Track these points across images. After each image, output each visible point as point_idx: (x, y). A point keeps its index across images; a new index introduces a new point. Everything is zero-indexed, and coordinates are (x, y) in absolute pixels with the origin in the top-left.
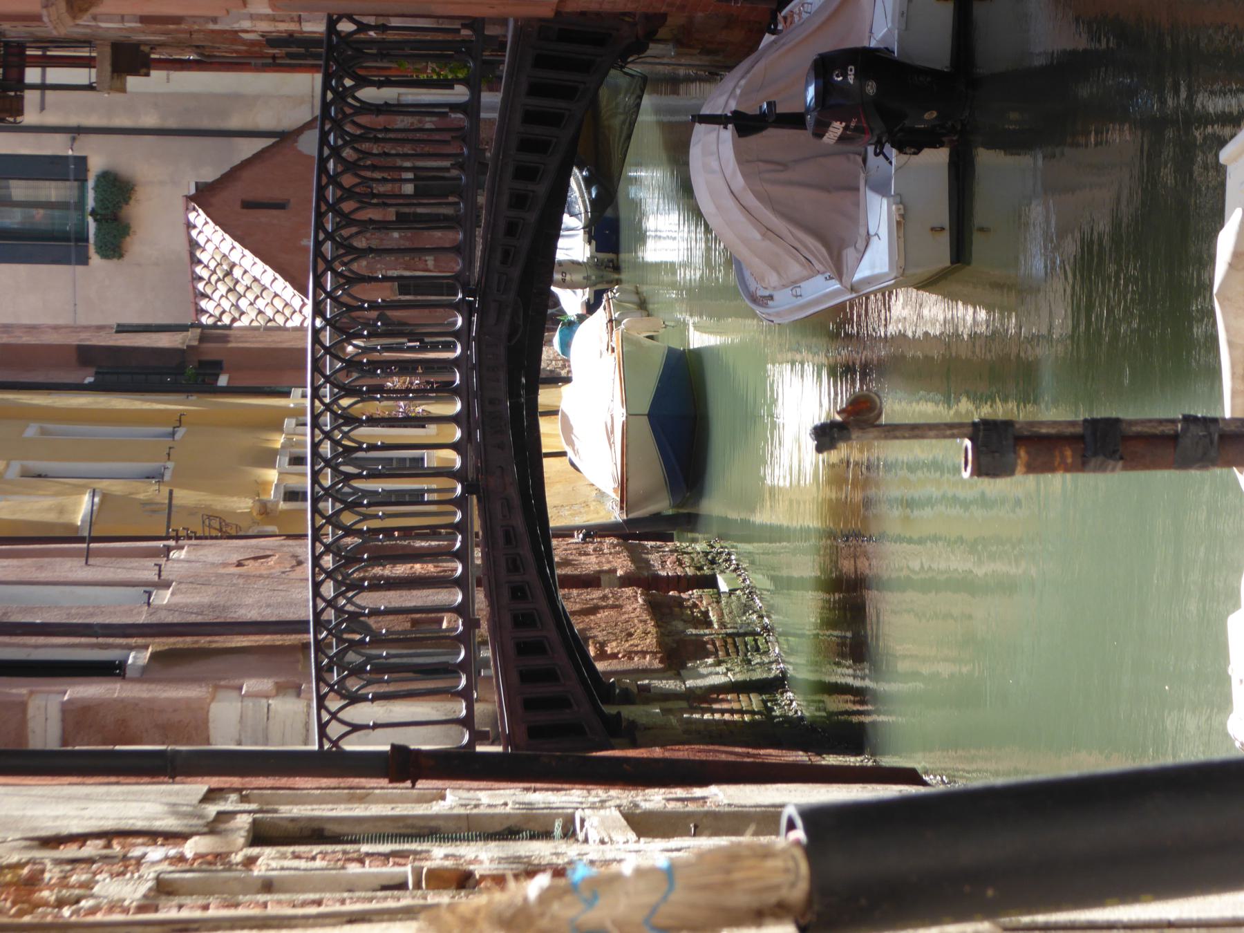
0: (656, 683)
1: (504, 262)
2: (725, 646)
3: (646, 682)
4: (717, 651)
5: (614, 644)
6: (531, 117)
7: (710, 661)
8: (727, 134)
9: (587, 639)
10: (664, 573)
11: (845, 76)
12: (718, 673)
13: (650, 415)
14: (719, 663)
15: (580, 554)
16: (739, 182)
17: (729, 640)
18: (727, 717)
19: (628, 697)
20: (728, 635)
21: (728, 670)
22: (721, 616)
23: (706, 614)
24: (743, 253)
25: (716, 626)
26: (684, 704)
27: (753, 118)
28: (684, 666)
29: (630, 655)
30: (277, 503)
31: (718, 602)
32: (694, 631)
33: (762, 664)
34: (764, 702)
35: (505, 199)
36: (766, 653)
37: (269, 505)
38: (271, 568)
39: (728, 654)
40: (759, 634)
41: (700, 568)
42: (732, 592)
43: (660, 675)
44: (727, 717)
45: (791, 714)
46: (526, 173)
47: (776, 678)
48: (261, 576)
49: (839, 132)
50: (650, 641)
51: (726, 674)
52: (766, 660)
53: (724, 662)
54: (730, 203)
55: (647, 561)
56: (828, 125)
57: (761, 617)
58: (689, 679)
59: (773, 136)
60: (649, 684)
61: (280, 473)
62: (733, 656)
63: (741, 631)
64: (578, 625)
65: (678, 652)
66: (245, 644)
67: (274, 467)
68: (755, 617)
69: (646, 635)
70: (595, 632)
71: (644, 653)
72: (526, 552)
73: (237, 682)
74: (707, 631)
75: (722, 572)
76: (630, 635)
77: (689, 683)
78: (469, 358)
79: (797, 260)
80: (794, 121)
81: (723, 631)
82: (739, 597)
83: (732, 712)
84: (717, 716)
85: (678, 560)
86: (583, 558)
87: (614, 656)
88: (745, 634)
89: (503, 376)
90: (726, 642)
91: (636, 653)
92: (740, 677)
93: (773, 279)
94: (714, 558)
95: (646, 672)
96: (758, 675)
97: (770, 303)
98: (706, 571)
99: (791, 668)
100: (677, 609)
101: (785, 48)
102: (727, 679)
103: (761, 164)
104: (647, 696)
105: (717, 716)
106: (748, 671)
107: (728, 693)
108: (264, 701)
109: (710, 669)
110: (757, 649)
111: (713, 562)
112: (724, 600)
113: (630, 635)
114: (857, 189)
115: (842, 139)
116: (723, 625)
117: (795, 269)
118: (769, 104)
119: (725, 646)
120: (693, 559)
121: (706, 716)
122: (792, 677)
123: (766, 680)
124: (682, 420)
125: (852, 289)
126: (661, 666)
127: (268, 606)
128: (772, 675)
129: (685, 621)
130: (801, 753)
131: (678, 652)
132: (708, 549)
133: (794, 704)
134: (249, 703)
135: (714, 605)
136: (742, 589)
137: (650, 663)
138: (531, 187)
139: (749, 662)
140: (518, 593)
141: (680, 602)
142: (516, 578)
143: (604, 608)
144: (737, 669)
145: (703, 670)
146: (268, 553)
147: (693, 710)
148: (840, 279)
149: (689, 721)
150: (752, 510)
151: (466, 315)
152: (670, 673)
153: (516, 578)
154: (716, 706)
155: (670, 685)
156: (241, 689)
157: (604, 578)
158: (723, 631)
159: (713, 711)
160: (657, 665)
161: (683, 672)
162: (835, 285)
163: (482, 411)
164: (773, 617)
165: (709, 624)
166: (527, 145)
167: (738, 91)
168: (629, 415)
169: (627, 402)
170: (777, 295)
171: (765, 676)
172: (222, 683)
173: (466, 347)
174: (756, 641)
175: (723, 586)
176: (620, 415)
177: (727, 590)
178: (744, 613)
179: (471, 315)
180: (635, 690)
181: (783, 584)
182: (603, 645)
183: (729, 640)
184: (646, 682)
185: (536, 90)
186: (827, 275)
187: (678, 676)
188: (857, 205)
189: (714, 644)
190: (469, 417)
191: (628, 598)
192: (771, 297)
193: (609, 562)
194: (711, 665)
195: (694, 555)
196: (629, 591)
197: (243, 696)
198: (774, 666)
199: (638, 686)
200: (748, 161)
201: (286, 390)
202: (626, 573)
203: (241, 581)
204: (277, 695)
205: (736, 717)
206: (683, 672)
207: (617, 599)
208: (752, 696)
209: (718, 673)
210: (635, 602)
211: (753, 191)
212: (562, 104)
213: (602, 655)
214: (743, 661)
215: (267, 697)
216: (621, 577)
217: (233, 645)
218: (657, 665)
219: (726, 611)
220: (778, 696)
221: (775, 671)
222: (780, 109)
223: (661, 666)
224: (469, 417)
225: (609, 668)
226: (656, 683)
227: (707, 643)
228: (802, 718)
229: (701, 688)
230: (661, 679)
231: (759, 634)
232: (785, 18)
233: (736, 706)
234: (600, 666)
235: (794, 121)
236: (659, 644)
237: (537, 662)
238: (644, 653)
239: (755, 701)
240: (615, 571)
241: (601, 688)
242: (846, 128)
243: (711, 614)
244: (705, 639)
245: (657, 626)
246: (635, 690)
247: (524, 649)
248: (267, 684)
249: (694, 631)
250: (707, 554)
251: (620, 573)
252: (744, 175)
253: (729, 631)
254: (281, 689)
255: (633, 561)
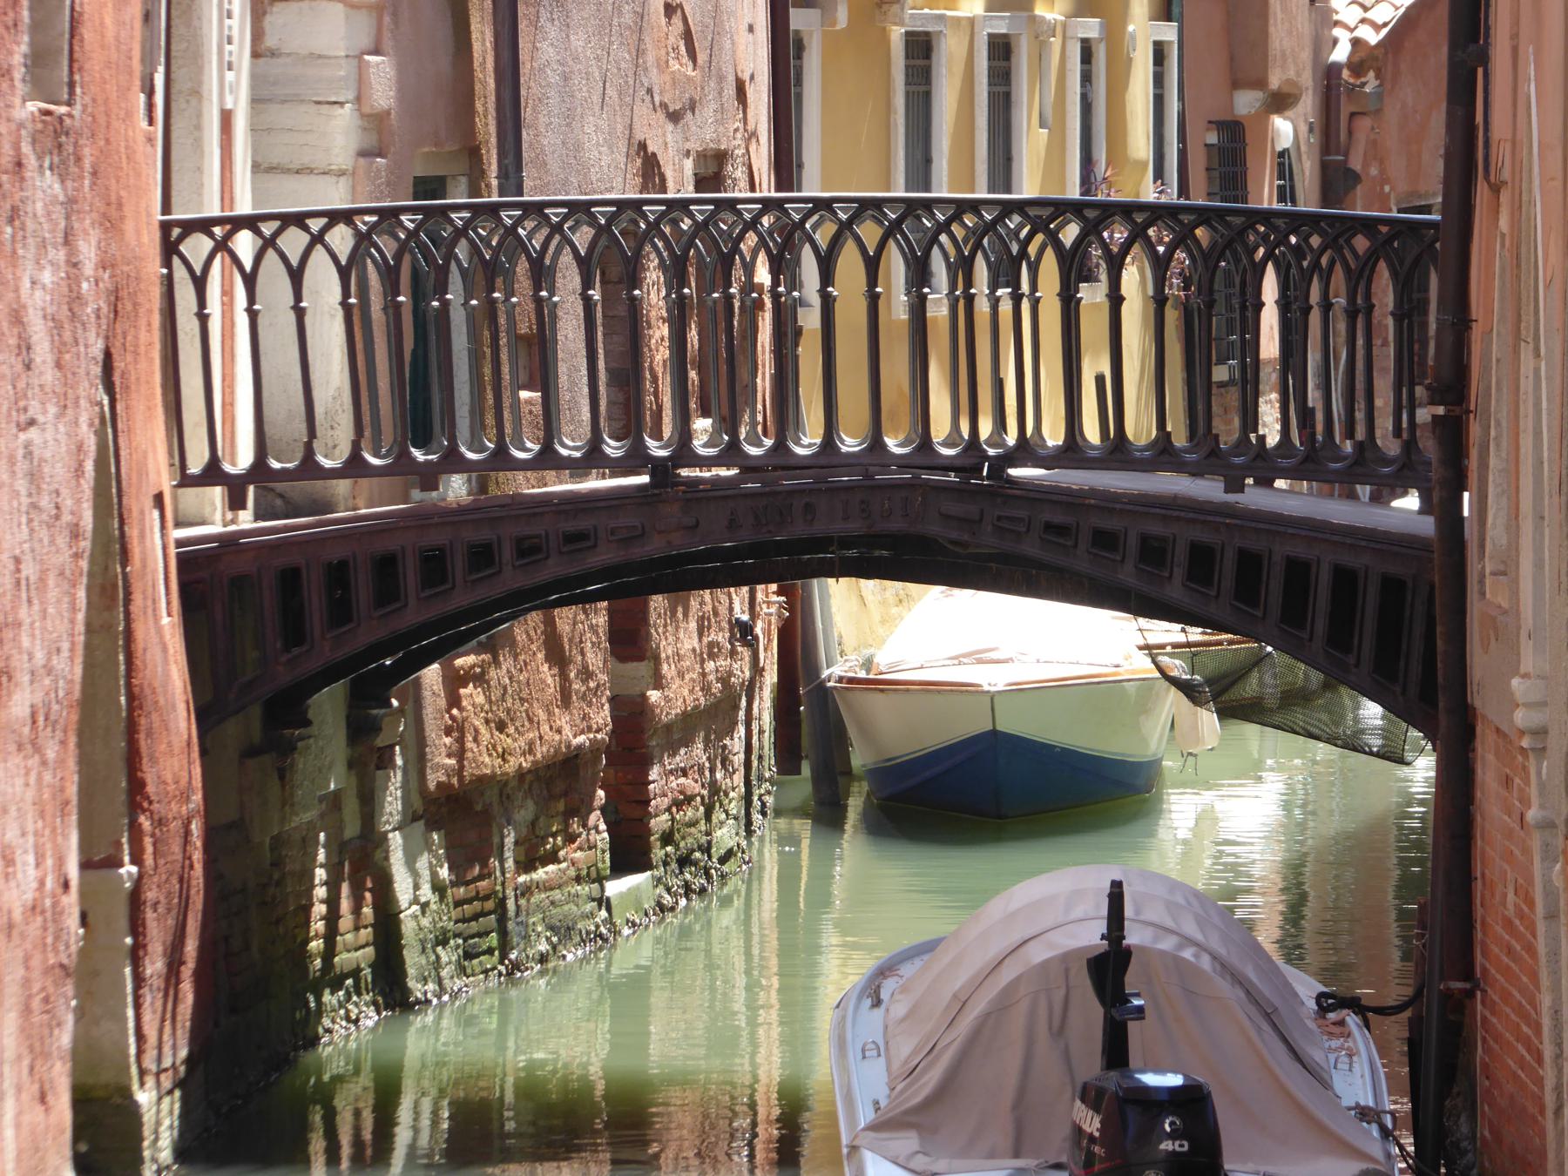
0: (396, 779)
1: (1049, 527)
2: (477, 897)
3: (399, 761)
4: (467, 883)
5: (480, 699)
6: (1298, 573)
7: (444, 872)
8: (1092, 935)
9: (491, 648)
10: (654, 773)
11: (1173, 1136)
12: (416, 887)
13: (994, 733)
14: (438, 888)
15: (701, 620)
16: (1038, 954)
17: (490, 905)
18: (320, 909)
19: (361, 729)
20: (502, 903)
21: (424, 907)
22: (546, 887)
23: (552, 858)
24: (943, 957)
25: (522, 879)
26: (352, 829)
27: (1120, 985)
28: (432, 825)
29: (457, 729)
30: (902, 24)
31: (578, 879)
32: (509, 841)
33: (437, 965)
34: (356, 973)
35: (1156, 529)
36: (462, 971)
37: (895, 8)
38: (663, 66)
39: (458, 904)
40: (504, 957)
41: (667, 839)
42: (603, 902)
43: (414, 784)
44: (320, 909)
45: (326, 1022)
46: (1202, 562)
47: (406, 991)
48: (640, 52)
49: (1086, 1128)
50: (487, 763)
51: (415, 901)
52: (444, 973)
53: (442, 898)
54: (1016, 937)
55: (687, 742)
56: (1096, 1108)
57: (543, 959)
58: (405, 838)
59: (1090, 1014)
60: (394, 766)
61: (972, 21)
62: (455, 914)
63: (511, 925)
64: (527, 629)
65: (462, 817)
66: (476, 46)
67: (988, 10)
68: (543, 947)
69: (498, 754)
70: (507, 663)
71: (460, 753)
72: (553, 568)
73: (388, 44)
74: (510, 864)
75: (659, 880)
76: (501, 727)
77: (396, 839)
78: (885, 467)
79: (915, 1052)
80: (1116, 1051)
81: (510, 893)
82: (592, 915)
83: (332, 918)
84: (321, 892)
85: (689, 799)
86: (693, 625)
87: (454, 701)
88: (503, 933)
89: (855, 527)
90: (487, 898)
91: (461, 741)
92: (408, 927)
93: (899, 1009)
94: (695, 863)
95: (419, 760)
96: (413, 960)
97: (869, 1002)
98: (658, 853)
99: (430, 1018)
100: (561, 806)
101: (1253, 1034)
102: (404, 903)
103: (1062, 992)
104: (368, 761)
105: (321, 892)
106: (423, 942)
107: (375, 907)
108: (351, 95)
109: (426, 874)
110: (469, 955)
111: (684, 861)
112: (584, 889)
113: (501, 727)
114: (1017, 1155)
115: (1078, 1130)
116: (526, 891)
117: (905, 1048)
118: (1140, 1009)
119: (477, 897)
120: (693, 824)
121: (320, 874)
122: (410, 1024)
123: (403, 974)
124: (993, 787)
125: (854, 1149)
126: (432, 786)
127: (566, 78)
128: (411, 983)
129: (533, 823)
130: (183, 1053)
131: (462, 817)
132: (717, 852)
133: (348, 1032)
134: (344, 70)
135: (572, 873)
136: (610, 921)
137: (438, 767)
138: (1179, 573)
139: (442, 941)
140: (483, 556)
141: (580, 810)
142: (507, 553)
143: (564, 676)
144: (425, 922)
145: (423, 863)
146: (702, 57)
147: (339, 849)
148: (873, 1127)
149: (308, 845)
150: (843, 928)
151: (958, 463)
152: (418, 804)
153: (507, 553)
154: (345, 888)
155: (393, 803)
156: (376, 52)
157: (642, 669)
158: (510, 893)
159: (333, 885)
160: (433, 779)
161: (420, 825)
162: (865, 1116)
163: (792, 492)
164: (542, 982)
165: (526, 865)
166: (1250, 564)
167: (1188, 954)
168: (992, 696)
169: (1018, 692)
170: (879, 1013)
171: (411, 971)
172: (387, 19)
173: (903, 463)
174: (490, 951)
175: (614, 888)
176: (992, 679)
177: (608, 893)
178: (551, 928)
179: (956, 470)
180: (381, 741)
181: (628, 996)
182: (480, 679)
183: (490, 905)
184: (399, 761)
185: (1345, 580)
186: (883, 1104)
187: (410, 818)
188: (992, 1155)
189: (481, 877)
190: (784, 468)
191: (585, 717)
192: (877, 1003)
193: (681, 675)
194: (434, 875)
195: (702, 826)
196: (602, 716)
197: (359, 57)
198: (431, 986)
199: (392, 747)
200: (1067, 970)
201: (1176, 10)
202: (652, 708)
203: (628, 18)
204: (363, 116)
205: (318, 926)
206: (420, 825)
207: (583, 698)
208: (370, 950)
209: (416, 887)
210: (583, 726)
211: (1018, 979)
212: (1321, 625)
213: (455, 682)
214: (444, 931)
215: (358, 99)
216: (644, 697)
217: (475, 26)
218: (433, 779)
219: (557, 895)
220: (368, 998)
221: (417, 989)
222: (1133, 1027)
223: (432, 786)
224: (784, 468)
225: (427, 694)
226: (396, 779)
227: (484, 864)
228: (314, 1041)
229: (387, 858)
230: (405, 786)
231: (504, 957)
232: (1342, 1023)
233: (346, 922)
234: (432, 674)
235: (1116, 1051)
236: (482, 781)
237: (363, 588)
238: (460, 753)
239: (356, 952)
240: (659, 683)
241: (374, 686)
242: (1091, 1138)
243: (551, 868)
244: (494, 862)
245: (521, 774)
246: (381, 741)
247: (387, 566)
248: (383, 94)
249: (509, 841)
250: (707, 849)
251: (654, 696)
252: (1045, 964)
253: (511, 904)
254: (375, 122)
255: (685, 715)
